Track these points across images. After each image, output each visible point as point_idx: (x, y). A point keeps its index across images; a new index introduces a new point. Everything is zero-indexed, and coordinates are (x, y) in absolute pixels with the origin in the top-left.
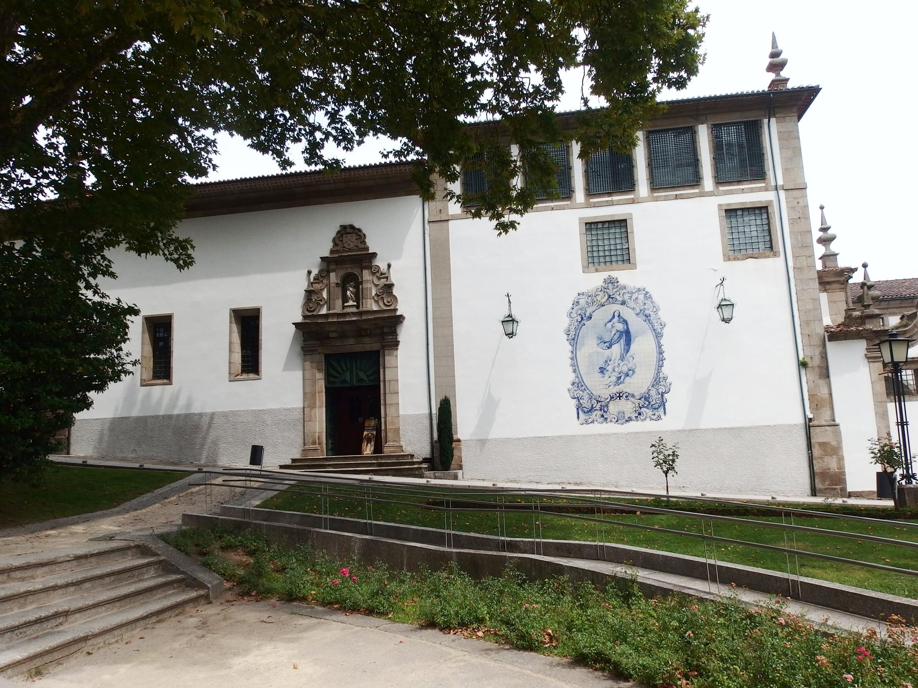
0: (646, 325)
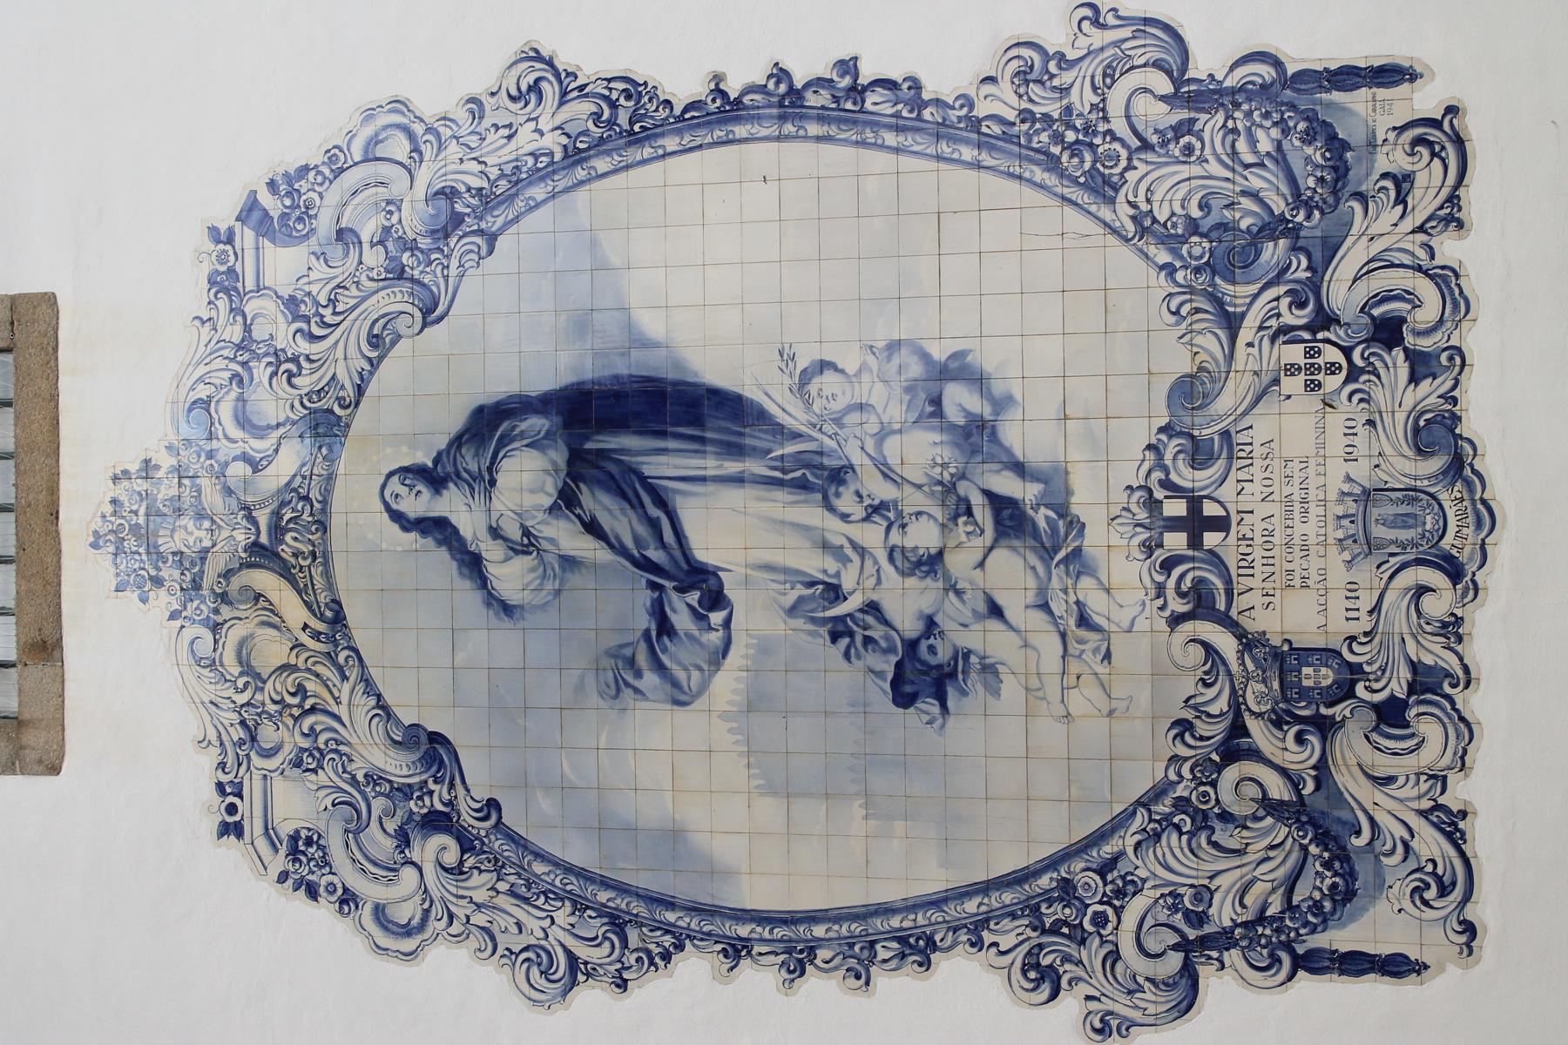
0: (532, 236)
